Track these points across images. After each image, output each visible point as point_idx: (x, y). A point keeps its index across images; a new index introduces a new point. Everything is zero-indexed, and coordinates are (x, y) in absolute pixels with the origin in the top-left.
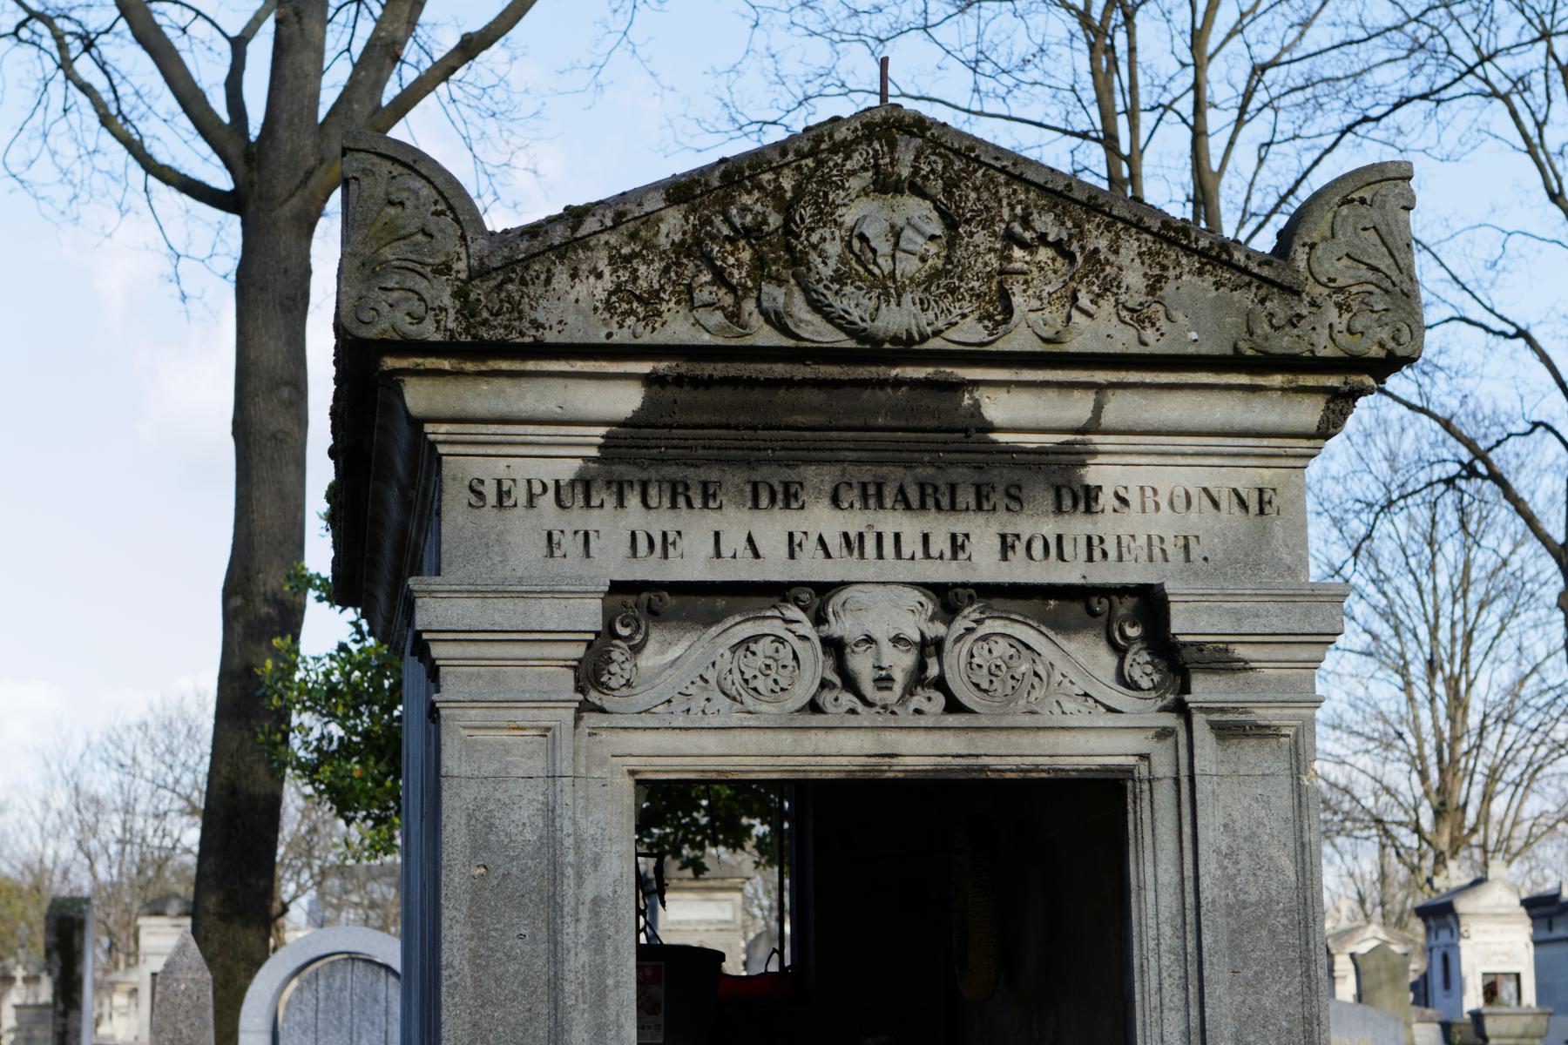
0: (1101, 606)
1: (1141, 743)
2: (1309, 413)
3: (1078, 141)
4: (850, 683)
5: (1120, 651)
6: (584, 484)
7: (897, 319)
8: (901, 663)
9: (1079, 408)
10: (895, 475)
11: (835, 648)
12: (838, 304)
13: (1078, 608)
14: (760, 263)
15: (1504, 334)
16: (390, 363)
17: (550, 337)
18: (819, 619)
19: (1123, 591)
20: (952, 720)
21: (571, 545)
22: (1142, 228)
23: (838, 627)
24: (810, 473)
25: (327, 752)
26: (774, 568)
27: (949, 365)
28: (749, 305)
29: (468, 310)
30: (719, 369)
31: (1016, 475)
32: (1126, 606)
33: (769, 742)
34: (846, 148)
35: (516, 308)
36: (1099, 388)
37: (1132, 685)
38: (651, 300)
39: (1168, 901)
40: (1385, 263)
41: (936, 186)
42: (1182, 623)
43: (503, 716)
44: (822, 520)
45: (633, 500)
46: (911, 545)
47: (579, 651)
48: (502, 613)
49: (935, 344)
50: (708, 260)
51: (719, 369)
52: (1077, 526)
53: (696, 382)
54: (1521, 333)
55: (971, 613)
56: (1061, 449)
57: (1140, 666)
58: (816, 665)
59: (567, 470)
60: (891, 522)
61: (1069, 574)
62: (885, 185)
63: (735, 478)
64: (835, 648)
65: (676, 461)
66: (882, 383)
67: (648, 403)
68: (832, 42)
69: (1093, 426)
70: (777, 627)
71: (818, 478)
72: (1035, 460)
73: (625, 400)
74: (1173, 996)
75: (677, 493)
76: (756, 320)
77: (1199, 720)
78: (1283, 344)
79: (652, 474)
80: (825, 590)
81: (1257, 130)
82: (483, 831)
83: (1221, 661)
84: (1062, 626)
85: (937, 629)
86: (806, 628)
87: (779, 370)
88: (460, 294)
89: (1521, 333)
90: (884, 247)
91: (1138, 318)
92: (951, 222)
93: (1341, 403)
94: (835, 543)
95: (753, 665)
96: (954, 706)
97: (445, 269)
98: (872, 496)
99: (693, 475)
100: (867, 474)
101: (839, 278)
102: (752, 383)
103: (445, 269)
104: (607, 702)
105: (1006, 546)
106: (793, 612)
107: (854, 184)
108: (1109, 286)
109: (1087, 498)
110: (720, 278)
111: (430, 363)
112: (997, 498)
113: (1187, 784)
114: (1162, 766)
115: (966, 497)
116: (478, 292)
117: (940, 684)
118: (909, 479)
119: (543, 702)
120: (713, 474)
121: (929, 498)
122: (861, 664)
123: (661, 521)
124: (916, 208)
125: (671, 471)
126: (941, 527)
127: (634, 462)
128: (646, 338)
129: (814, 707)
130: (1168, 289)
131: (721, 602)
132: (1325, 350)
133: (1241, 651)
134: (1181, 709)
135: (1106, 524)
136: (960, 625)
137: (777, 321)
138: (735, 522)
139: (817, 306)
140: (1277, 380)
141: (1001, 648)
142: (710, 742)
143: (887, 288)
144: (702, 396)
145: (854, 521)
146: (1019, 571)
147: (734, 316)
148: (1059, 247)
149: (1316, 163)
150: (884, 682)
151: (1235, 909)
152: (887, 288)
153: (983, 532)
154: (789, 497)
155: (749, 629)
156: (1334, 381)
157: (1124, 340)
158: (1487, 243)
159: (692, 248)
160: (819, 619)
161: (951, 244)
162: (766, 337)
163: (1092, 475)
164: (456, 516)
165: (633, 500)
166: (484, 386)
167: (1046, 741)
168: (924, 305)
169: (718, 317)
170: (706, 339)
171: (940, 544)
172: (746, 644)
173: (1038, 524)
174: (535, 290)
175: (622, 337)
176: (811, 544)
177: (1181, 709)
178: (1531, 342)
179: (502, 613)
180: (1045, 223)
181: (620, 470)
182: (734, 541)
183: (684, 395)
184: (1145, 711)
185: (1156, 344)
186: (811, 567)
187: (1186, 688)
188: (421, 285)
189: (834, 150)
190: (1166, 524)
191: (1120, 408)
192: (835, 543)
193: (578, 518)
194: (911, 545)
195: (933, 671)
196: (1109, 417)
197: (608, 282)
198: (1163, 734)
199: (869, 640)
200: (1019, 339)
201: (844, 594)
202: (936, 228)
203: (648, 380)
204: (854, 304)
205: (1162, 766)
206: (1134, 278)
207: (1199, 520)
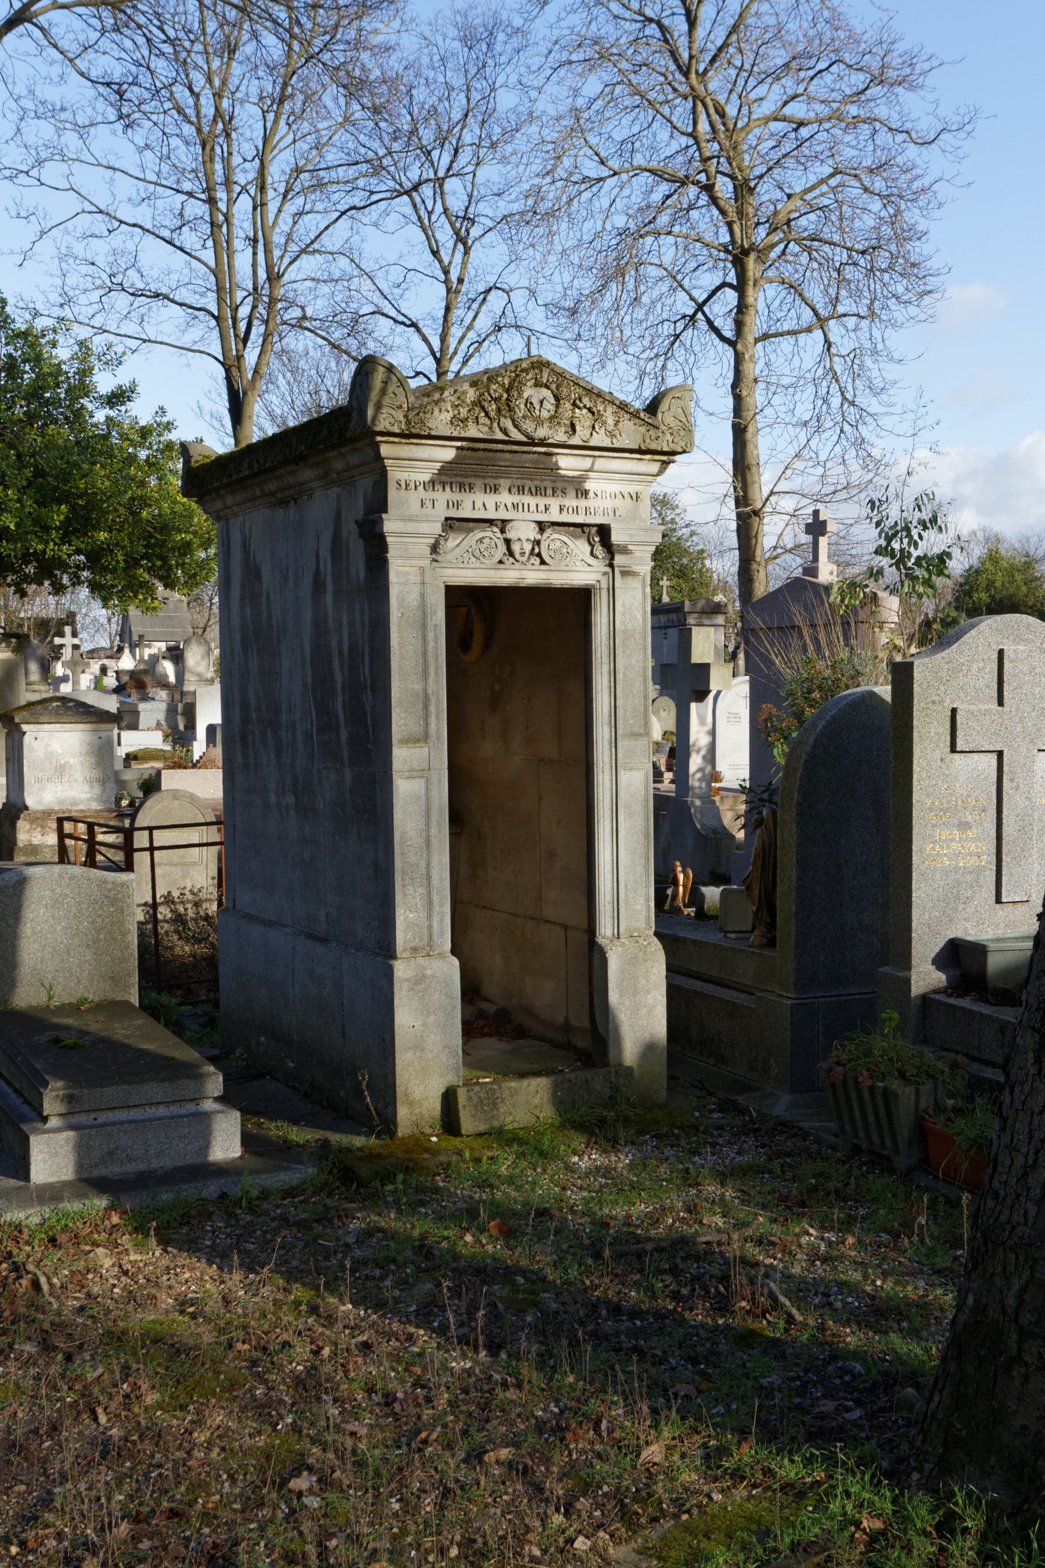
0: (587, 530)
1: (599, 577)
2: (655, 467)
3: (185, 197)
4: (511, 554)
5: (592, 546)
6: (433, 482)
7: (541, 433)
8: (528, 547)
9: (587, 463)
10: (528, 483)
12: (524, 427)
13: (579, 530)
14: (499, 410)
15: (403, 323)
16: (379, 438)
17: (433, 433)
18: (503, 531)
19: (593, 526)
20: (543, 567)
21: (429, 504)
22: (613, 403)
23: (511, 535)
24: (502, 481)
26: (491, 514)
28: (495, 425)
29: (408, 422)
30: (482, 445)
31: (565, 485)
32: (594, 530)
33: (487, 573)
34: (525, 370)
35: (422, 422)
36: (594, 457)
38: (464, 421)
39: (605, 629)
40: (684, 420)
41: (553, 387)
42: (616, 538)
43: (408, 562)
44: (506, 498)
45: (448, 489)
46: (533, 508)
47: (432, 541)
48: (411, 527)
49: (550, 441)
50: (483, 408)
51: (482, 445)
52: (582, 503)
53: (473, 449)
54: (414, 325)
55: (549, 531)
56: (579, 477)
57: (599, 550)
58: (502, 548)
59: (426, 477)
60: (527, 499)
61: (579, 519)
62: (538, 384)
63: (479, 483)
64: (508, 542)
65: (462, 476)
66: (529, 453)
67: (457, 456)
68: (57, 129)
69: (591, 470)
70: (490, 534)
71: (504, 483)
72: (570, 480)
73: (448, 454)
74: (605, 659)
75: (461, 487)
76: (497, 430)
77: (617, 570)
78: (654, 446)
79: (454, 480)
80: (505, 522)
81: (291, 208)
82: (402, 600)
83: (625, 550)
84: (574, 536)
85: (538, 537)
86: (499, 535)
87: (500, 447)
88: (406, 416)
89: (414, 325)
90: (537, 407)
91: (612, 436)
92: (557, 398)
93: (665, 464)
94: (510, 506)
95: (482, 547)
96: (543, 562)
97: (400, 407)
98: (521, 490)
99: (466, 481)
100: (519, 482)
101: (524, 417)
102: (490, 450)
103: (400, 407)
104: (439, 558)
105: (561, 510)
106: (495, 529)
107: (529, 384)
108: (604, 423)
109: (585, 493)
110: (487, 415)
111: (392, 439)
112: (559, 492)
113: (612, 591)
115: (549, 492)
116: (411, 415)
117: (539, 555)
118: (532, 484)
119: (422, 557)
120: (472, 480)
121: (538, 492)
122: (516, 548)
123: (456, 496)
124: (546, 393)
125: (460, 479)
126: (542, 501)
127: (447, 475)
128: (463, 435)
129: (501, 562)
130: (620, 425)
131: (471, 524)
132: (666, 449)
133: (630, 547)
134: (611, 565)
135: (591, 503)
136: (546, 535)
137: (505, 432)
138: (480, 497)
139: (516, 426)
140: (648, 457)
141: (558, 544)
142: (469, 573)
143: (539, 422)
144: (474, 454)
145: (516, 499)
147: (491, 428)
148: (590, 410)
149: (327, 228)
150: (523, 554)
151: (625, 632)
152: (539, 422)
153: (554, 503)
154: (495, 489)
155: (481, 535)
156: (665, 458)
157: (606, 442)
158: (396, 274)
159: (478, 403)
160: (503, 531)
161: (557, 406)
162: (500, 436)
163: (588, 485)
164: (393, 494)
165: (448, 489)
166: (406, 447)
167: (570, 575)
168: (550, 428)
169: (486, 429)
170: (481, 436)
171: (542, 508)
172: (481, 540)
173: (571, 502)
174: (428, 416)
175: (455, 434)
176: (502, 506)
177: (611, 565)
178: (418, 330)
179: (411, 527)
180: (586, 401)
181: (444, 478)
182: (479, 505)
183: (468, 453)
185: (617, 445)
186: (502, 514)
187: (612, 558)
188: (393, 412)
189: (522, 371)
190: (609, 504)
191: (600, 464)
192: (510, 506)
193: (431, 495)
194: (533, 508)
195: (537, 550)
196: (596, 468)
197: (451, 414)
198: (605, 574)
200: (576, 441)
202: (553, 401)
203: (458, 448)
204: (529, 426)
205: (604, 585)
206: (610, 421)
207: (619, 503)
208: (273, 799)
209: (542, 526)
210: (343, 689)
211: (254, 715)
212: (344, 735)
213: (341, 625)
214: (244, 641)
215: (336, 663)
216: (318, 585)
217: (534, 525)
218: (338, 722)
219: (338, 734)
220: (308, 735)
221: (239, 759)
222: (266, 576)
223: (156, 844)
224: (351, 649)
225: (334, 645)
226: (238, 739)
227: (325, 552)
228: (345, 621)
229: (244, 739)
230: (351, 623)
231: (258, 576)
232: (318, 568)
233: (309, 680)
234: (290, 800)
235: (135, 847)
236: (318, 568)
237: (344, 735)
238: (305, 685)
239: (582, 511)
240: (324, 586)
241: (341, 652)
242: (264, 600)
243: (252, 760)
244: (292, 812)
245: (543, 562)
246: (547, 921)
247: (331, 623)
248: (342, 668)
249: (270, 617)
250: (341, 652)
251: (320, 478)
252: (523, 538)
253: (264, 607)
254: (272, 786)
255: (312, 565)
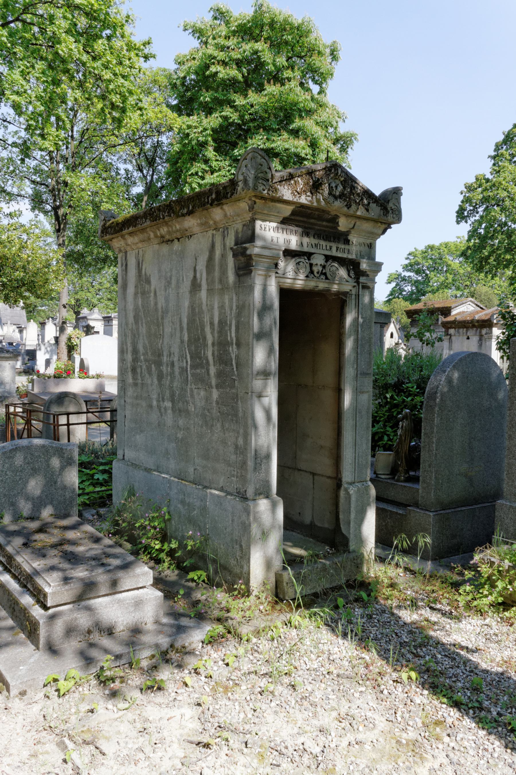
11: (311, 265)
23: (312, 261)
25: (44, 375)
27: (120, 325)
37: (351, 277)
45: (285, 232)
55: (330, 261)
57: (352, 274)
60: (323, 243)
77: (361, 285)
94: (314, 245)
96: (327, 278)
113: (358, 296)
114: (354, 292)
115: (332, 239)
117: (325, 274)
126: (329, 244)
136: (329, 263)
146: (340, 255)
153: (334, 246)
160: (309, 259)
171: (328, 248)
177: (358, 282)
184: (352, 283)
187: (358, 279)
192: (314, 245)
194: (324, 248)
199: (317, 265)
201: (314, 255)
205: (354, 292)
208: (155, 403)
209: (328, 258)
210: (213, 344)
211: (142, 357)
212: (213, 370)
213: (213, 308)
214: (136, 318)
215: (208, 329)
216: (195, 286)
217: (323, 257)
218: (208, 363)
219: (208, 371)
220: (183, 370)
221: (130, 380)
222: (154, 282)
223: (70, 422)
224: (220, 322)
225: (206, 319)
226: (129, 370)
227: (201, 266)
228: (216, 306)
229: (134, 370)
230: (222, 307)
231: (148, 281)
232: (195, 277)
233: (186, 338)
234: (168, 404)
235: (60, 423)
236: (195, 277)
237: (213, 370)
238: (182, 342)
239: (346, 251)
240: (200, 286)
241: (212, 324)
242: (152, 294)
243: (140, 381)
244: (170, 411)
245: (327, 278)
246: (300, 470)
247: (204, 307)
248: (212, 333)
249: (156, 304)
250: (212, 324)
251: (202, 224)
252: (319, 264)
253: (152, 298)
254: (155, 396)
255: (191, 275)
